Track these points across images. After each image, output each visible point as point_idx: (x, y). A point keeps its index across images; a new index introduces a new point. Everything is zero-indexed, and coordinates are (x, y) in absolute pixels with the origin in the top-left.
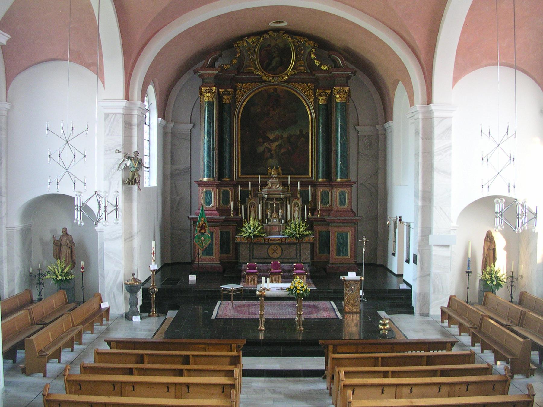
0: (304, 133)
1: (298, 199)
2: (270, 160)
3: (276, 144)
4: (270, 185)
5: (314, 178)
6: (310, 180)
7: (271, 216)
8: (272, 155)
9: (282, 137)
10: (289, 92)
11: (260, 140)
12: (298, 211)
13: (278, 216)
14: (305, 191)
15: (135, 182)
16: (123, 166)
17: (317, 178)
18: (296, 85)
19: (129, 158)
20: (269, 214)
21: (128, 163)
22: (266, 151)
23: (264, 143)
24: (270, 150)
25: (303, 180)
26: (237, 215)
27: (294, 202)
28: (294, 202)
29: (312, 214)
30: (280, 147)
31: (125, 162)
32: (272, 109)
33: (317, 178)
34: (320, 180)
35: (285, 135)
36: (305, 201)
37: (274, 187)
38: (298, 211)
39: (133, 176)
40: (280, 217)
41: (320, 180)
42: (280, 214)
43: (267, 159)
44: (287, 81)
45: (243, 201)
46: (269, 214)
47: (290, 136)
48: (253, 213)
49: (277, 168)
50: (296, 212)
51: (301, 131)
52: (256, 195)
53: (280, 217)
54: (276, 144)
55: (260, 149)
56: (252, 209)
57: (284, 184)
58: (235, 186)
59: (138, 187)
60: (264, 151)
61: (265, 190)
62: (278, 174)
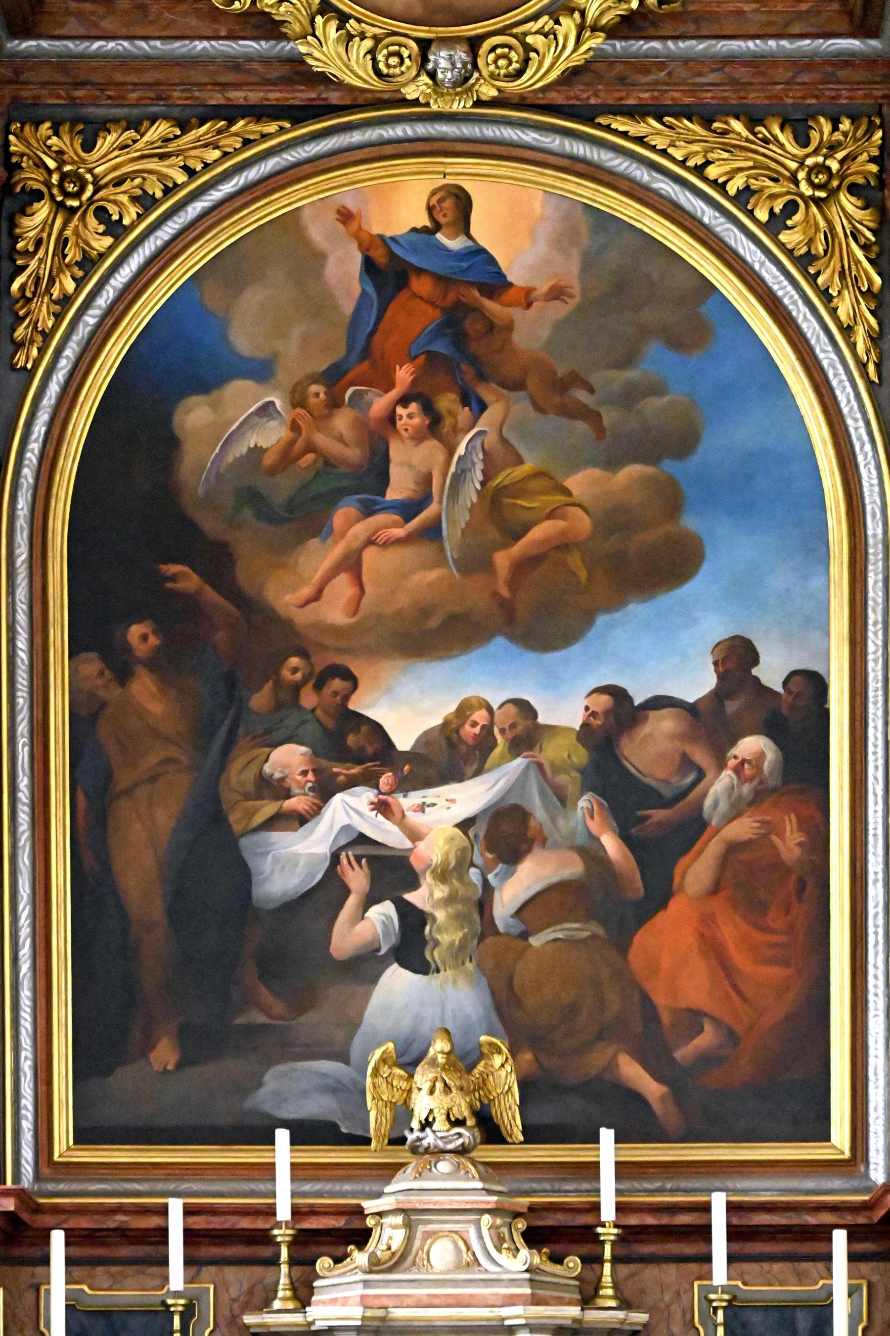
0: (771, 671)
2: (396, 980)
3: (470, 796)
4: (389, 1236)
6: (837, 1190)
8: (413, 921)
9: (527, 731)
10: (601, 220)
11: (289, 759)
14: (783, 1312)
18: (684, 141)
22: (357, 879)
23: (325, 790)
24: (392, 873)
25: (764, 1189)
30: (504, 834)
32: (410, 417)
35: (565, 709)
43: (365, 967)
44: (576, 100)
47: (620, 713)
49: (465, 1060)
51: (737, 657)
54: (470, 796)
55: (287, 861)
57: (555, 1233)
60: (328, 892)
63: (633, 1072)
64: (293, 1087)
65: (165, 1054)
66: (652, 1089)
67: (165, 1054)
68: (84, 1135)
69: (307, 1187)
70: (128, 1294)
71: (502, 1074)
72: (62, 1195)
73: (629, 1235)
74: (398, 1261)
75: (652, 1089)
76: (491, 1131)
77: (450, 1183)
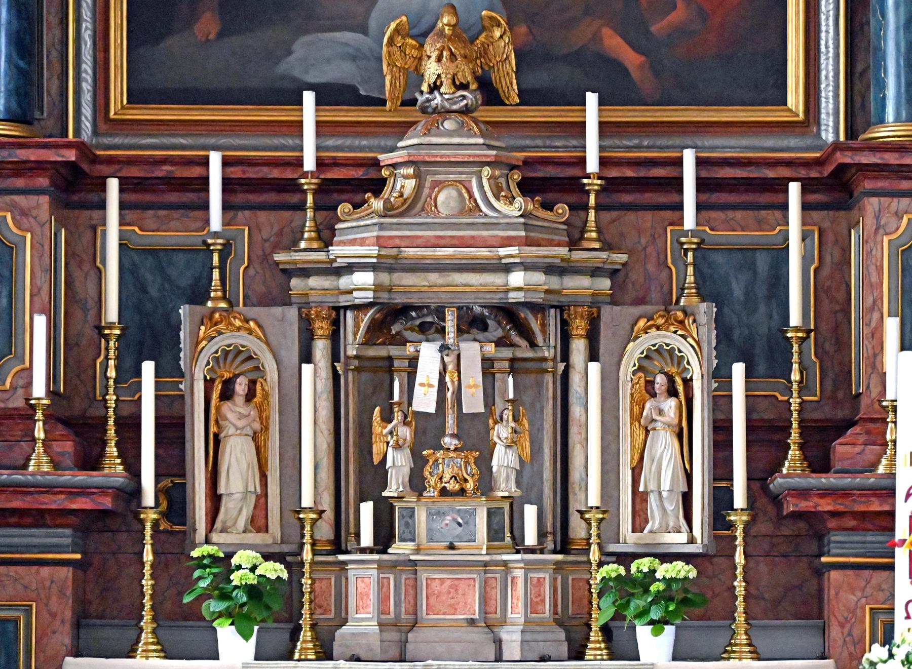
1: (669, 311)
5: (831, 129)
6: (792, 146)
7: (417, 483)
12: (683, 435)
13: (486, 484)
14: (747, 252)
17: (859, 110)
20: (398, 464)
26: (91, 461)
27: (634, 351)
28: (634, 351)
29: (819, 462)
33: (859, 110)
34: (890, 129)
36: (753, 340)
37: (455, 215)
38: (683, 435)
40: (506, 487)
41: (890, 129)
42: (503, 459)
45: (147, 334)
46: (398, 464)
48: (238, 456)
49: (467, 35)
50: (664, 446)
52: (275, 288)
53: (506, 487)
56: (236, 414)
57: (547, 182)
58: (75, 187)
61: (358, 237)
62: (490, 94)
63: (615, 44)
64: (319, 55)
65: (208, 24)
66: (631, 58)
67: (208, 24)
68: (136, 97)
69: (331, 142)
70: (172, 234)
71: (502, 44)
72: (118, 145)
73: (611, 185)
74: (408, 207)
75: (631, 58)
76: (490, 94)
77: (453, 139)
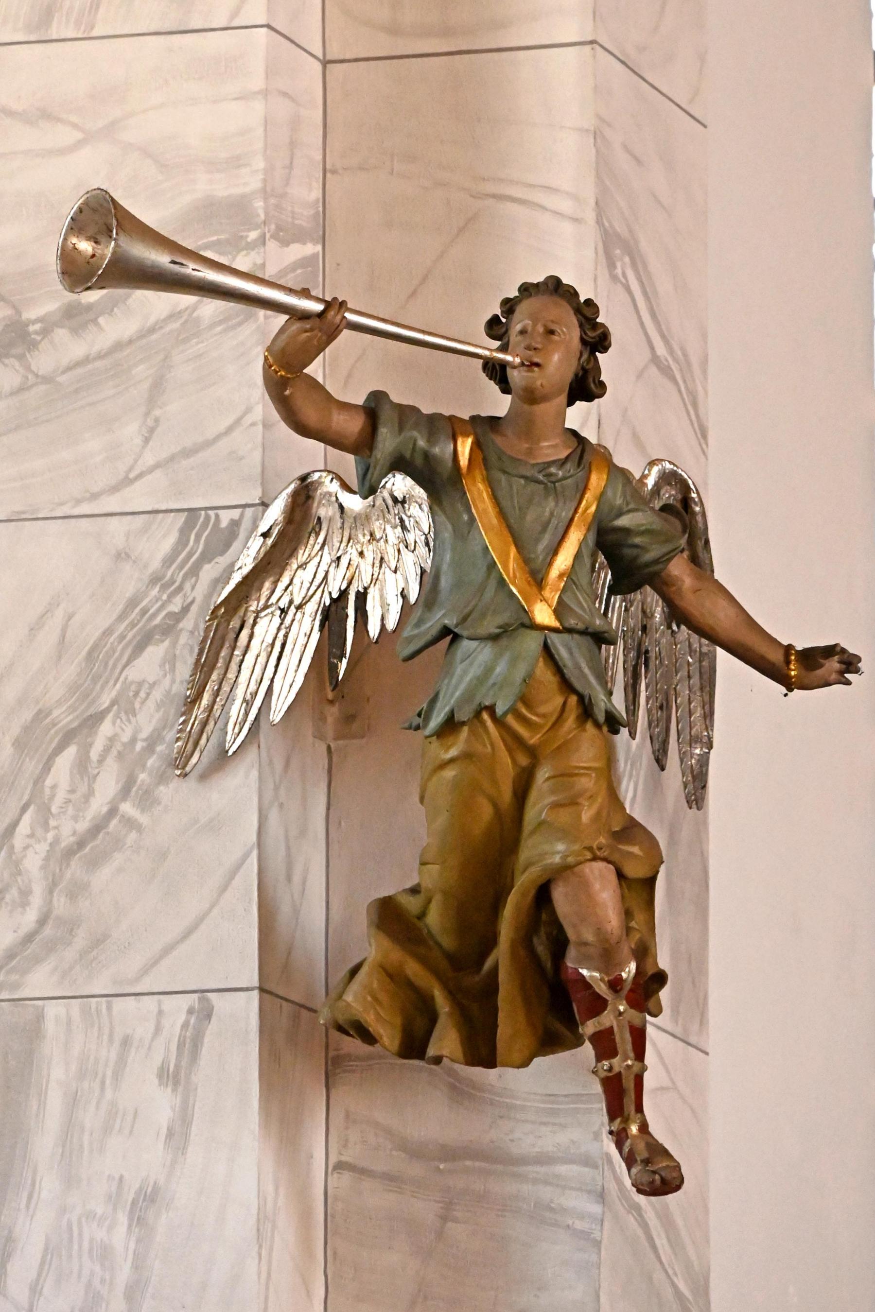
15: (559, 1012)
16: (278, 659)
19: (380, 439)
21: (386, 556)
31: (311, 576)
39: (488, 860)
59: (622, 1097)
